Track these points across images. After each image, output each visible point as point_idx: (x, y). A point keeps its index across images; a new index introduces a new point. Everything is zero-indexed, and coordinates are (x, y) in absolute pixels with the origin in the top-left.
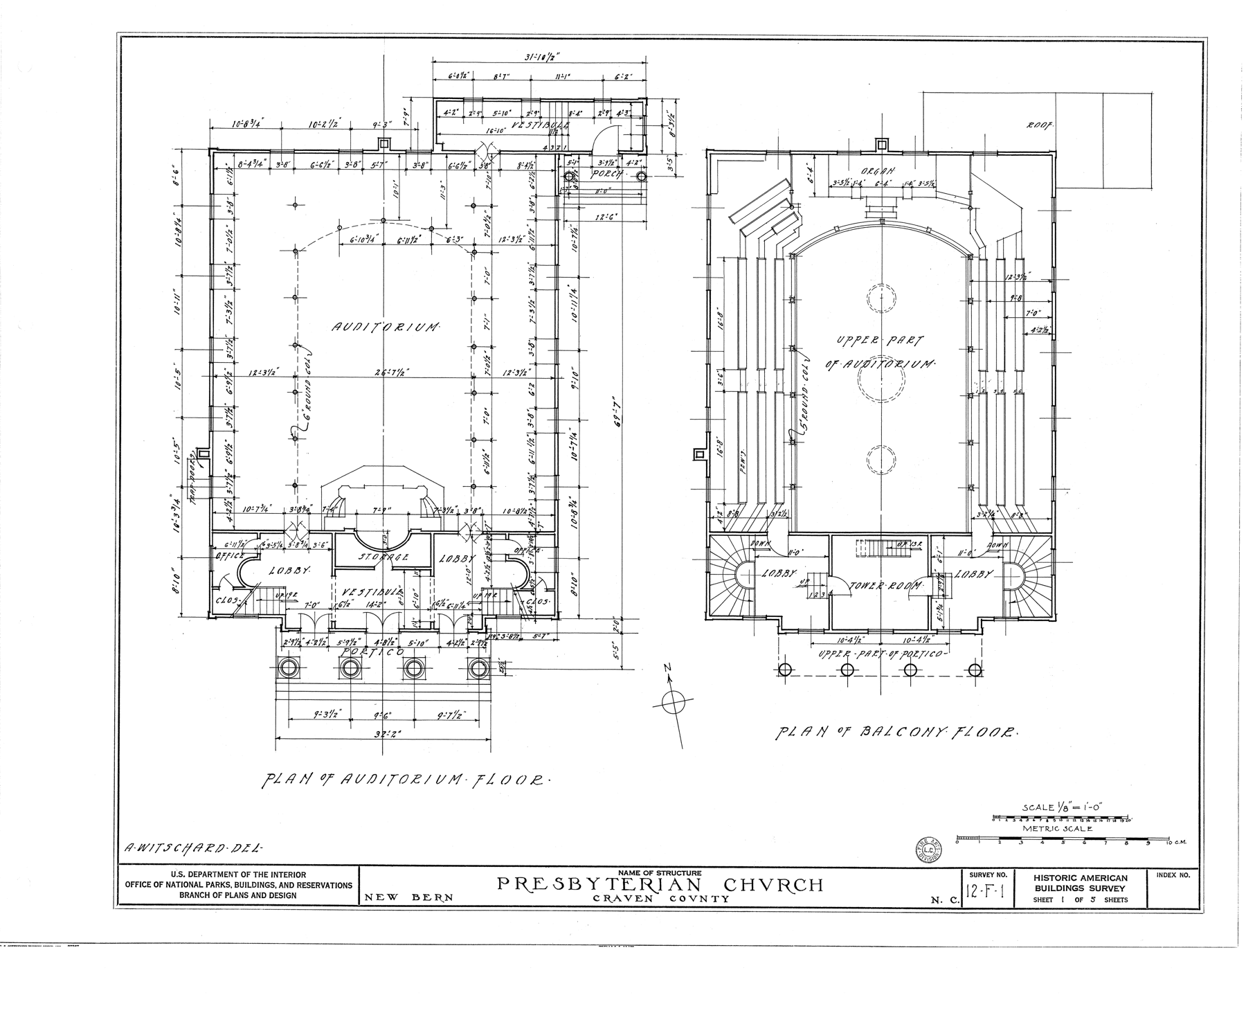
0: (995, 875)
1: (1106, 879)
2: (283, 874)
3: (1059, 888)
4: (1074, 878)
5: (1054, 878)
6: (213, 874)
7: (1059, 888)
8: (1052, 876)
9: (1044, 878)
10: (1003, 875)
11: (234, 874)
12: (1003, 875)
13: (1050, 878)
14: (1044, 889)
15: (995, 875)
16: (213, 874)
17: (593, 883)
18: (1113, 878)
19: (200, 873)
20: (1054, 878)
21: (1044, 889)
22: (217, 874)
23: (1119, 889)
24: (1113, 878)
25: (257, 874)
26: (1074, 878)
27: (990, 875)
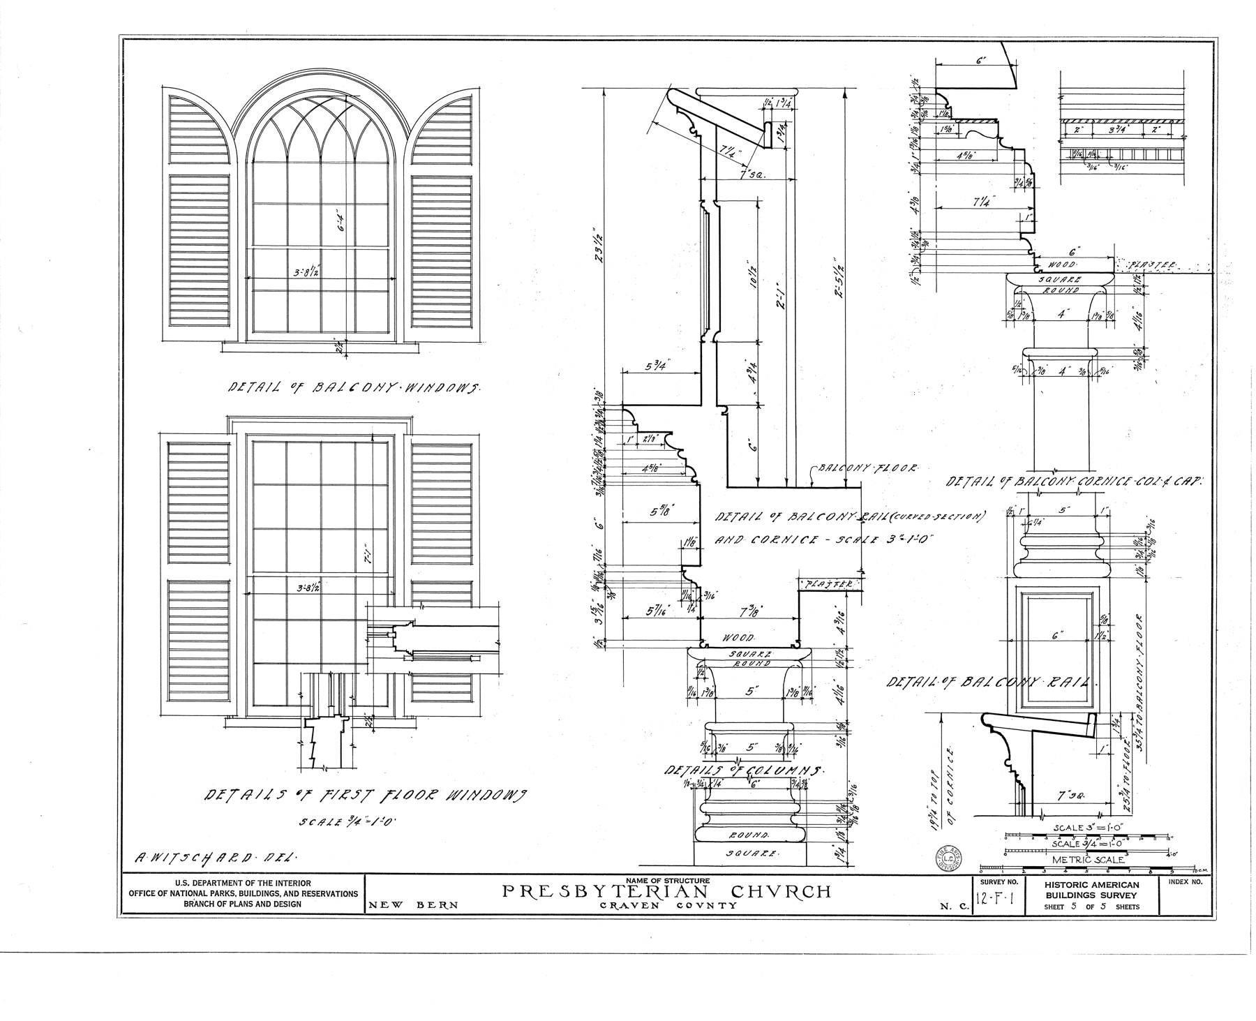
0: (1006, 882)
1: (1079, 886)
2: (287, 883)
3: (1070, 895)
4: (1085, 885)
5: (1065, 884)
6: (217, 882)
7: (1070, 895)
8: (1063, 883)
9: (1055, 885)
10: (1014, 882)
11: (238, 883)
13: (1061, 885)
14: (1110, 896)
15: (1006, 882)
16: (217, 882)
18: (1124, 885)
19: (204, 882)
20: (1065, 884)
21: (1110, 896)
22: (221, 882)
23: (1131, 896)
24: (1124, 885)
26: (1085, 885)
27: (1001, 882)
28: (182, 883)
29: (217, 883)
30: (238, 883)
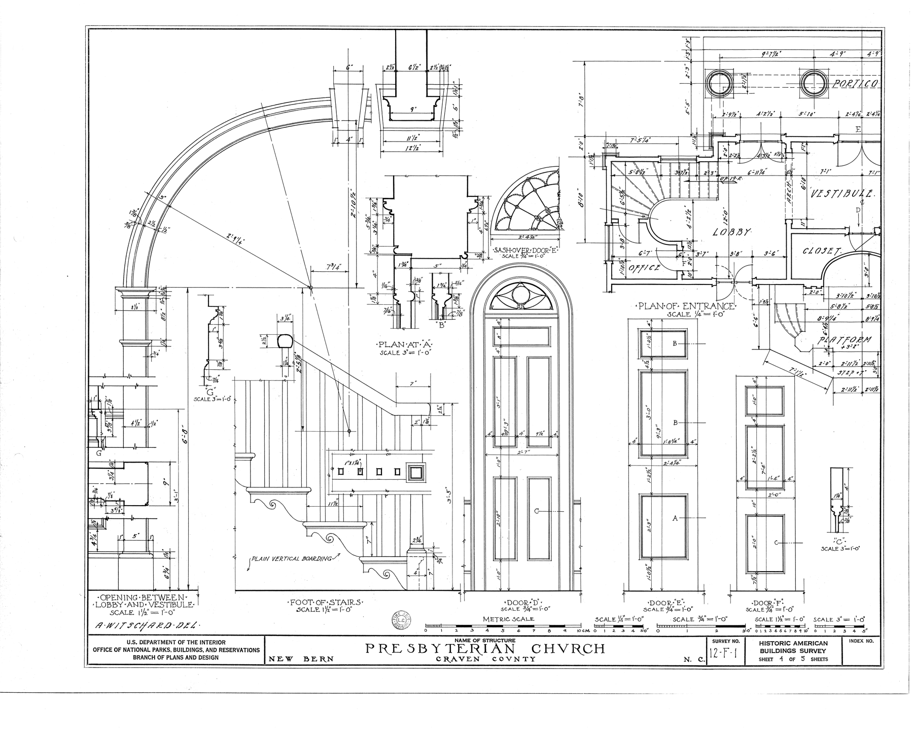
0: (731, 641)
2: (208, 642)
3: (778, 651)
4: (788, 643)
5: (774, 643)
7: (778, 651)
8: (772, 642)
9: (766, 644)
10: (737, 641)
11: (173, 642)
12: (871, 641)
13: (771, 643)
14: (767, 651)
15: (731, 641)
17: (436, 648)
18: (817, 643)
19: (148, 641)
20: (774, 643)
22: (160, 642)
23: (822, 651)
24: (817, 643)
25: (190, 642)
26: (788, 643)
27: (728, 641)
28: (131, 642)
29: (157, 643)
30: (173, 642)
